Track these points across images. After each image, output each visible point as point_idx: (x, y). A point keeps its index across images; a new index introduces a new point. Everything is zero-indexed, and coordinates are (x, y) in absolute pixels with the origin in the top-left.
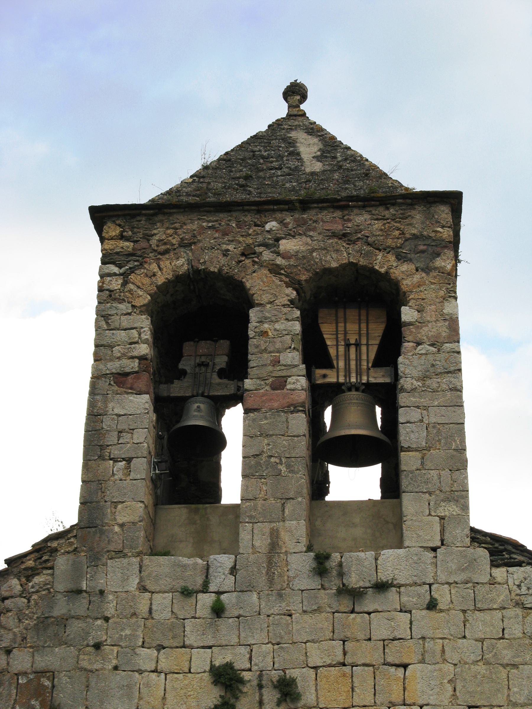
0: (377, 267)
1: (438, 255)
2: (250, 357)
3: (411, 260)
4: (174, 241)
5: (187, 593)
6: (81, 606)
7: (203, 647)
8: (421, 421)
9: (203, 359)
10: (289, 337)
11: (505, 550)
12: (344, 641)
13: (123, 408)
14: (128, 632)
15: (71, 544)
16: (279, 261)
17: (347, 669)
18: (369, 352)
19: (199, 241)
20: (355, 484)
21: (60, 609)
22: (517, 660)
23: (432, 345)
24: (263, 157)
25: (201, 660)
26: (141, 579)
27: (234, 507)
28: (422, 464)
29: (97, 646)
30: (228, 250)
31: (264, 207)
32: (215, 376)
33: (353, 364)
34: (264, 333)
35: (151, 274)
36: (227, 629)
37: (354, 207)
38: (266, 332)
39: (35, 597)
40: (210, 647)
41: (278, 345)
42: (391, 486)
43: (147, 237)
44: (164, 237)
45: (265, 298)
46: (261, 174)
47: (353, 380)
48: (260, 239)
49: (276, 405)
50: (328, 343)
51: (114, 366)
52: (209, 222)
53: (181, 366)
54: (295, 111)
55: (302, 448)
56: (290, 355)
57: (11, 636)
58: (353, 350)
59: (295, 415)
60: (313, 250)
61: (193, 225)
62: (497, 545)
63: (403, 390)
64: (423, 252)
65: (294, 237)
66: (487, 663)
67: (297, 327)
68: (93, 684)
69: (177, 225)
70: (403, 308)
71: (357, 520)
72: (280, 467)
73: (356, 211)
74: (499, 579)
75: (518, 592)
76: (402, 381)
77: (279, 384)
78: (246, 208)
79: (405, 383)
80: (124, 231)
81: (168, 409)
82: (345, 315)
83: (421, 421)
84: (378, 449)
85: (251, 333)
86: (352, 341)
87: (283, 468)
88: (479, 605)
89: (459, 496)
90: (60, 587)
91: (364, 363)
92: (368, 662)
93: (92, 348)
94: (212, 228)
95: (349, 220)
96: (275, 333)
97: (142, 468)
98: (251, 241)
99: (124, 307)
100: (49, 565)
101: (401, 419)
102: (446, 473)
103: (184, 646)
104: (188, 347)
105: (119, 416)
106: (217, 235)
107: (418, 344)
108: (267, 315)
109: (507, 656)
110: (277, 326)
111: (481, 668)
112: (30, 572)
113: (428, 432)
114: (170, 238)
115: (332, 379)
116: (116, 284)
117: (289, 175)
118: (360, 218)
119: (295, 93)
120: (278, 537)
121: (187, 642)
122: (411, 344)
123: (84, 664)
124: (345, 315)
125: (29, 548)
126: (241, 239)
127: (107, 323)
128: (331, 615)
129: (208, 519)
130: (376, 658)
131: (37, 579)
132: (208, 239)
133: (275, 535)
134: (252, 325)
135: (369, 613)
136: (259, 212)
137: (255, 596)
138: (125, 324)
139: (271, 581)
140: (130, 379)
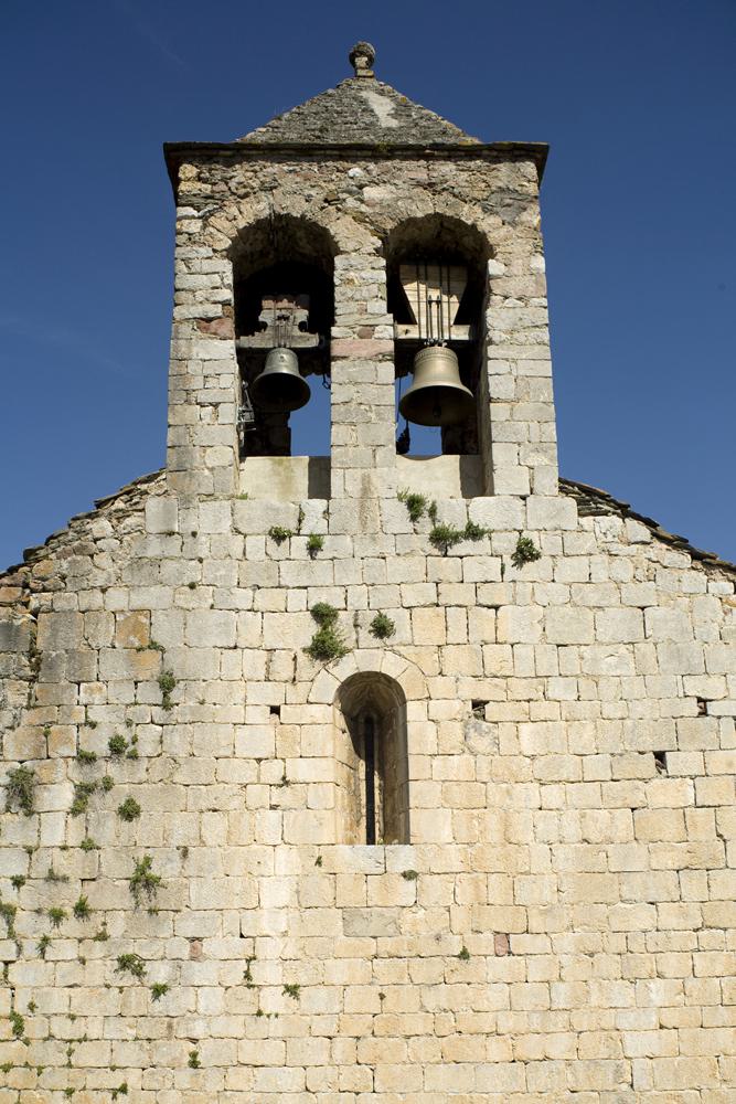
0: (463, 219)
1: (525, 209)
2: (336, 305)
3: (497, 213)
4: (254, 185)
5: (279, 536)
7: (299, 588)
8: (510, 373)
11: (592, 500)
12: (437, 584)
13: (208, 353)
14: (223, 572)
15: (161, 487)
16: (363, 208)
17: (441, 610)
18: (453, 305)
21: (154, 549)
22: (603, 603)
23: (520, 299)
24: (337, 112)
25: (298, 600)
28: (511, 415)
29: (192, 586)
32: (296, 328)
33: (435, 321)
34: (350, 281)
35: (231, 218)
36: (321, 566)
38: (352, 280)
39: (127, 538)
40: (306, 588)
41: (365, 294)
43: (226, 181)
44: (243, 179)
46: (335, 127)
47: (435, 336)
48: (344, 185)
49: (364, 353)
50: (410, 298)
52: (289, 166)
53: (261, 319)
57: (105, 575)
58: (434, 306)
59: (384, 363)
60: (398, 199)
63: (491, 342)
64: (509, 205)
65: (377, 184)
67: (383, 276)
68: (190, 622)
69: (257, 168)
70: (490, 261)
72: (369, 414)
74: (586, 528)
75: (605, 539)
77: (367, 331)
78: (328, 152)
79: (494, 335)
80: (201, 173)
81: (251, 361)
82: (426, 272)
87: (373, 415)
95: (434, 170)
96: (362, 281)
98: (334, 188)
99: (205, 251)
100: (139, 507)
102: (534, 425)
103: (279, 587)
106: (298, 179)
107: (506, 298)
108: (353, 262)
110: (363, 274)
112: (121, 514)
114: (250, 181)
118: (446, 169)
120: (369, 482)
121: (283, 583)
122: (498, 298)
124: (426, 272)
126: (323, 185)
128: (424, 559)
129: (292, 471)
130: (469, 599)
131: (128, 521)
132: (289, 183)
133: (366, 481)
135: (461, 557)
136: (341, 158)
137: (349, 539)
138: (206, 268)
139: (364, 524)
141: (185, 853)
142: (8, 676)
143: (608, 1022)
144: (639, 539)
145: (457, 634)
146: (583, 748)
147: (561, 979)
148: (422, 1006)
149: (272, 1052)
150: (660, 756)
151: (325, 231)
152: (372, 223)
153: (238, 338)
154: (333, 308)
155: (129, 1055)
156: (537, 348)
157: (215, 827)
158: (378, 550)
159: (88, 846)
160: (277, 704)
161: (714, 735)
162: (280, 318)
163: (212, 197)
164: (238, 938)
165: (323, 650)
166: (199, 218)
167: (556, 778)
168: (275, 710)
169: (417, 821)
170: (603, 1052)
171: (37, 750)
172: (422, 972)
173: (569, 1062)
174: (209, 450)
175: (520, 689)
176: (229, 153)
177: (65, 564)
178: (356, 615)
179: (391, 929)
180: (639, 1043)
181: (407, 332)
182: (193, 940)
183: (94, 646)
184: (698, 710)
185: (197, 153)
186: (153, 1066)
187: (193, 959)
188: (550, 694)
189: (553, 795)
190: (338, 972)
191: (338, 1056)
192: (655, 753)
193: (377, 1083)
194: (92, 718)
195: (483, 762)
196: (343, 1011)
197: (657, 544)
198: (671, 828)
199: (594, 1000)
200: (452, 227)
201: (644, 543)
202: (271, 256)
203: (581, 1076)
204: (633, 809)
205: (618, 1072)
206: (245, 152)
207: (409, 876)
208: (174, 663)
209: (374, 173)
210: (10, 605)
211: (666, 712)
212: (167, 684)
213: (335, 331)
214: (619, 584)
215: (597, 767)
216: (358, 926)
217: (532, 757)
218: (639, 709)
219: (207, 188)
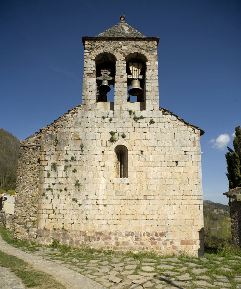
2: (116, 71)
6: (83, 119)
8: (150, 86)
9: (106, 72)
14: (93, 125)
15: (81, 108)
16: (122, 51)
17: (135, 133)
18: (139, 71)
21: (80, 120)
22: (167, 132)
26: (95, 115)
28: (150, 94)
29: (87, 127)
30: (111, 48)
32: (108, 76)
34: (119, 66)
39: (74, 118)
40: (109, 128)
43: (94, 45)
44: (98, 45)
46: (117, 33)
47: (136, 78)
48: (118, 46)
49: (121, 81)
50: (131, 70)
53: (101, 74)
57: (70, 125)
58: (136, 71)
60: (129, 49)
63: (146, 79)
64: (151, 50)
66: (161, 132)
67: (125, 65)
68: (86, 135)
69: (100, 42)
74: (164, 117)
77: (122, 77)
78: (115, 39)
79: (147, 78)
81: (99, 82)
82: (134, 64)
83: (150, 86)
85: (116, 66)
86: (136, 70)
87: (123, 94)
88: (160, 122)
90: (79, 116)
91: (138, 75)
92: (139, 131)
94: (108, 43)
95: (136, 43)
100: (77, 112)
101: (146, 85)
102: (154, 96)
103: (104, 128)
106: (109, 45)
107: (150, 70)
109: (165, 131)
110: (121, 65)
112: (73, 113)
113: (151, 88)
115: (131, 77)
117: (122, 34)
118: (139, 43)
123: (85, 131)
124: (134, 64)
130: (141, 131)
132: (107, 45)
133: (121, 107)
136: (117, 40)
137: (117, 119)
138: (90, 63)
139: (120, 116)
140: (92, 75)
141: (85, 179)
142: (51, 145)
144: (174, 119)
145: (138, 138)
147: (156, 204)
148: (130, 209)
149: (101, 217)
150: (177, 162)
151: (114, 55)
152: (123, 54)
155: (74, 217)
156: (156, 80)
157: (91, 174)
158: (123, 121)
159: (67, 178)
160: (103, 151)
163: (91, 48)
165: (112, 140)
166: (89, 52)
167: (156, 166)
168: (103, 152)
169: (129, 174)
170: (164, 218)
171: (57, 159)
172: (130, 202)
174: (90, 100)
175: (150, 149)
176: (95, 39)
177: (62, 123)
178: (119, 134)
179: (124, 194)
180: (170, 217)
181: (130, 77)
182: (86, 196)
184: (184, 153)
185: (88, 39)
187: (86, 199)
188: (156, 150)
189: (156, 169)
190: (114, 202)
191: (113, 218)
193: (121, 223)
194: (67, 153)
197: (178, 120)
198: (178, 176)
199: (162, 209)
200: (139, 55)
201: (175, 120)
202: (103, 61)
203: (159, 222)
205: (166, 222)
206: (98, 39)
207: (128, 184)
208: (84, 143)
209: (124, 43)
210: (52, 131)
212: (82, 147)
213: (116, 76)
214: (170, 128)
215: (164, 164)
216: (118, 194)
217: (152, 162)
218: (173, 153)
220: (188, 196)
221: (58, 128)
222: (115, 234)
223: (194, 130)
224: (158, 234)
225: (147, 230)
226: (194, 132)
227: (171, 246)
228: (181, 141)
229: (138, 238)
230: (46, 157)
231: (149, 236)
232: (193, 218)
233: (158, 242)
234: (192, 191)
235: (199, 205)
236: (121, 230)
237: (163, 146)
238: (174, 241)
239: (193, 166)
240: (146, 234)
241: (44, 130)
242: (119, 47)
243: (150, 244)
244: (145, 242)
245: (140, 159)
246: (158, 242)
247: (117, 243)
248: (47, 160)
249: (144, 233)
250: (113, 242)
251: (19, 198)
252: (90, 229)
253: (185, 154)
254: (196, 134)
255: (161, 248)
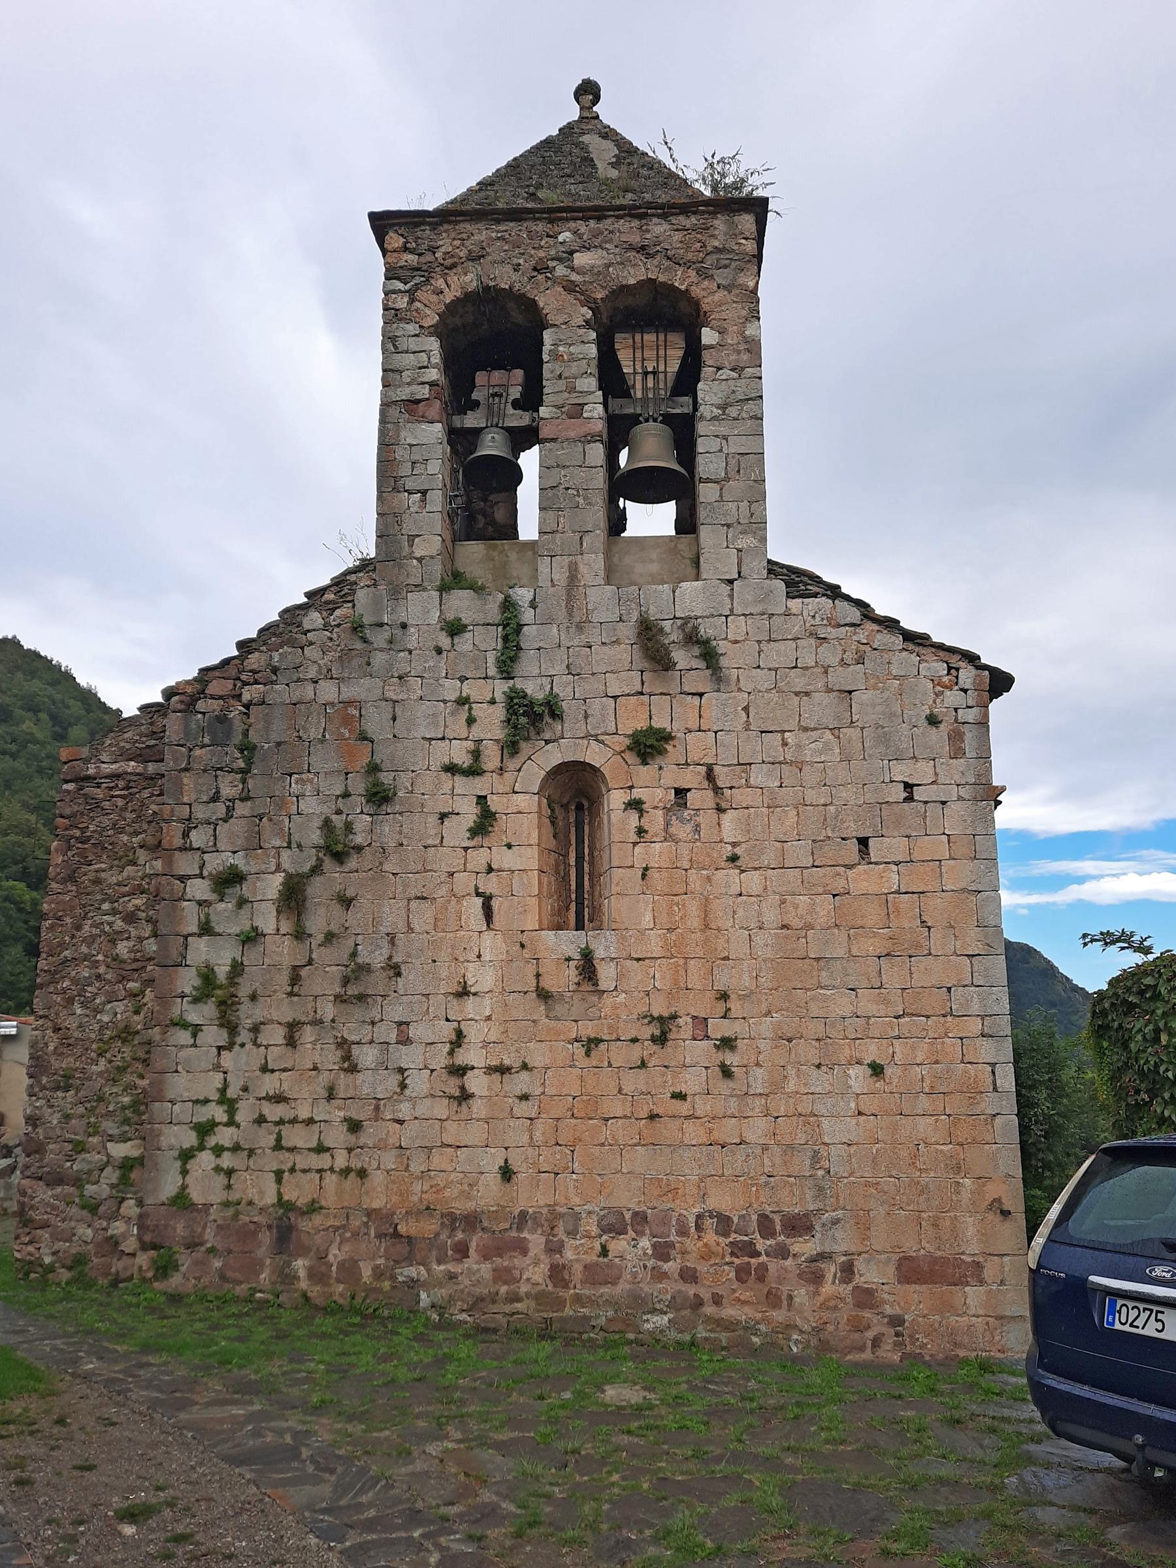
0: (676, 284)
2: (545, 383)
4: (462, 254)
8: (721, 451)
9: (496, 390)
10: (585, 361)
16: (574, 277)
17: (645, 698)
19: (488, 254)
20: (651, 520)
27: (532, 544)
28: (721, 496)
31: (555, 215)
32: (509, 406)
37: (653, 215)
42: (686, 524)
43: (433, 250)
45: (559, 319)
48: (553, 252)
49: (572, 434)
51: (404, 393)
52: (498, 232)
54: (587, 114)
55: (599, 480)
56: (586, 381)
58: (650, 378)
60: (608, 266)
61: (481, 233)
62: (793, 576)
67: (593, 350)
69: (464, 236)
71: (654, 556)
72: (577, 499)
73: (655, 220)
74: (794, 611)
75: (813, 622)
76: (701, 409)
77: (577, 411)
79: (705, 410)
81: (461, 441)
83: (721, 451)
84: (673, 485)
85: (545, 357)
89: (757, 527)
93: (380, 374)
95: (648, 231)
97: (436, 499)
99: (412, 328)
100: (350, 598)
101: (700, 449)
104: (480, 377)
105: (411, 445)
106: (506, 248)
107: (719, 369)
111: (774, 696)
112: (331, 606)
116: (402, 302)
118: (658, 228)
119: (588, 92)
120: (576, 569)
123: (390, 694)
125: (327, 582)
126: (533, 252)
127: (394, 345)
131: (337, 612)
134: (547, 348)
136: (551, 221)
137: (555, 630)
138: (413, 347)
139: (570, 615)
143: (804, 1108)
144: (848, 620)
146: (785, 834)
149: (475, 1133)
150: (863, 842)
153: (449, 416)
154: (543, 387)
157: (422, 917)
161: (919, 820)
162: (494, 395)
163: (418, 269)
164: (443, 1022)
169: (615, 907)
173: (765, 1148)
180: (838, 1130)
182: (400, 1024)
183: (305, 737)
186: (361, 1148)
188: (752, 781)
189: (753, 881)
191: (538, 1135)
192: (858, 839)
195: (684, 849)
196: (543, 1093)
197: (871, 626)
198: (873, 915)
199: (791, 1086)
204: (834, 896)
205: (815, 1157)
211: (870, 797)
215: (799, 853)
219: (412, 259)
220: (928, 1017)
221: (256, 682)
222: (546, 1224)
223: (957, 669)
224: (772, 1221)
225: (713, 1203)
226: (957, 683)
227: (846, 1290)
228: (885, 734)
229: (672, 1245)
230: (193, 835)
231: (726, 1234)
232: (962, 1134)
233: (773, 1266)
234: (949, 989)
235: (993, 1065)
236: (577, 1200)
237: (791, 763)
238: (860, 1265)
239: (951, 858)
240: (709, 1223)
241: (183, 698)
242: (560, 260)
243: (732, 1275)
244: (702, 1268)
245: (672, 830)
246: (773, 1266)
247: (557, 1273)
248: (198, 849)
249: (699, 1217)
250: (534, 1272)
251: (51, 1048)
252: (415, 1199)
253: (910, 799)
254: (965, 691)
255: (790, 1297)
